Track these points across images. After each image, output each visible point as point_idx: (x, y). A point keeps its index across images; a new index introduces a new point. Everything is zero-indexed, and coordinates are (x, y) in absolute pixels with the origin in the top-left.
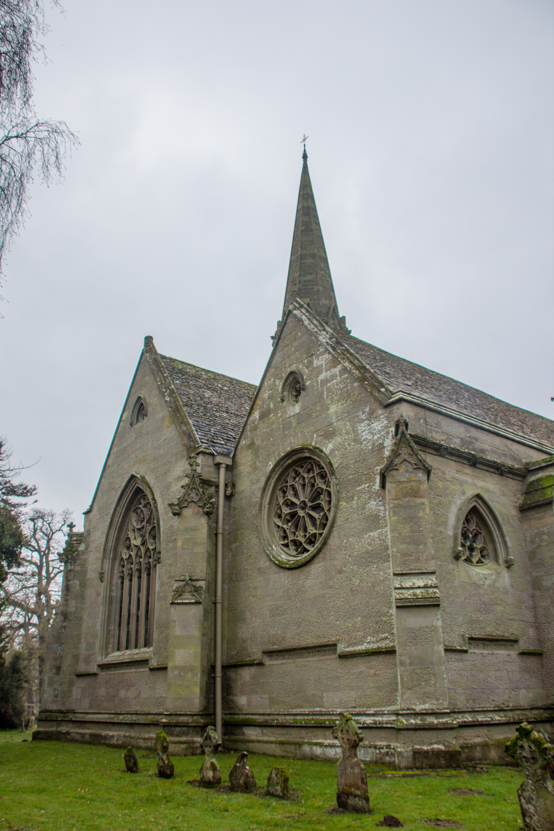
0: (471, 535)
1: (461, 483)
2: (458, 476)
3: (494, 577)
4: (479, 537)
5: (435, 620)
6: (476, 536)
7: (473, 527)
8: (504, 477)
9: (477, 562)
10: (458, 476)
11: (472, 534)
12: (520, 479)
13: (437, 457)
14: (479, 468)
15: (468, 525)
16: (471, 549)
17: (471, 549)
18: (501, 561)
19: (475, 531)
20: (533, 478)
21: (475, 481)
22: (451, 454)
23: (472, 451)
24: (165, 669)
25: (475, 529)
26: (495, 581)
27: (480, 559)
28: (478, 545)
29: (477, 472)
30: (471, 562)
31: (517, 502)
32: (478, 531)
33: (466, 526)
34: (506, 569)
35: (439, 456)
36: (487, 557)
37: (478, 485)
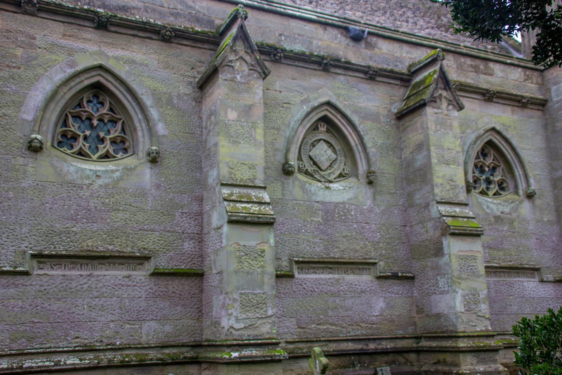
0: (487, 169)
1: (71, 52)
2: (63, 42)
3: (118, 174)
4: (498, 169)
5: (270, 237)
6: (494, 169)
7: (489, 161)
8: (173, 45)
9: (494, 194)
10: (63, 42)
11: (488, 167)
12: (211, 47)
13: (19, 16)
14: (495, 102)
15: (484, 159)
16: (489, 182)
17: (489, 182)
18: (521, 192)
19: (492, 165)
20: (418, 79)
21: (103, 48)
22: (55, 13)
23: (99, 8)
24: (278, 276)
25: (492, 163)
26: (120, 179)
27: (497, 191)
28: (497, 178)
29: (108, 37)
30: (487, 194)
31: (195, 77)
32: (495, 164)
33: (482, 160)
34: (149, 165)
35: (22, 13)
36: (507, 189)
37: (110, 54)
